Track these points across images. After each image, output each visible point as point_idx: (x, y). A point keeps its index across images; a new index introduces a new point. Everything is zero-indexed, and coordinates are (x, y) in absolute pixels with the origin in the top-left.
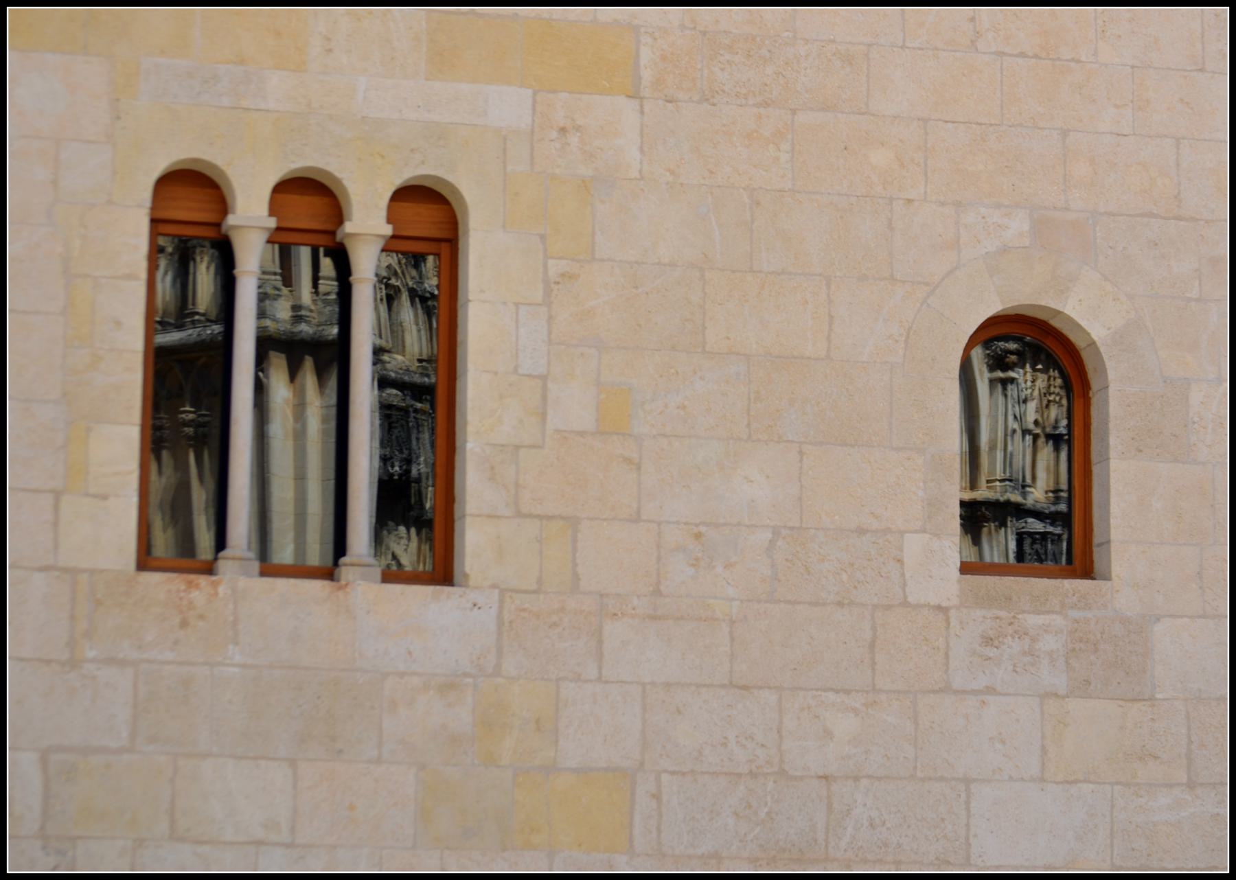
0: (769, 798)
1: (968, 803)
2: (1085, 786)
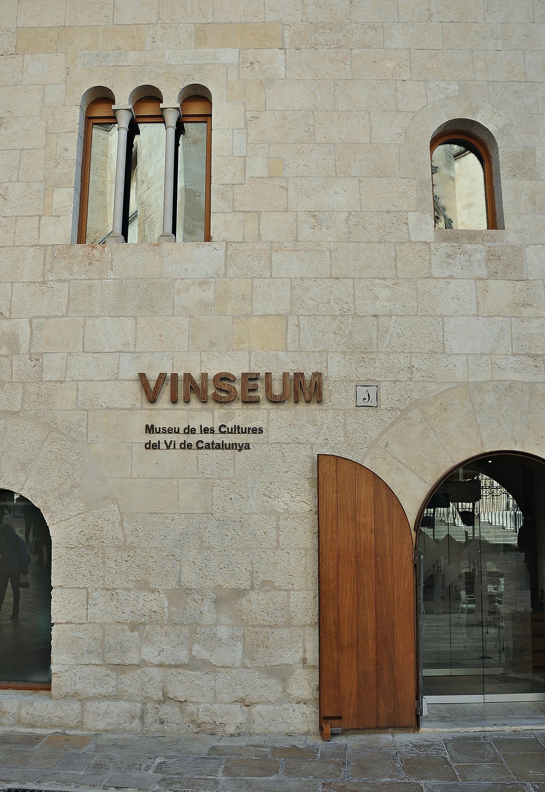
0: (350, 325)
1: (443, 326)
2: (498, 318)
